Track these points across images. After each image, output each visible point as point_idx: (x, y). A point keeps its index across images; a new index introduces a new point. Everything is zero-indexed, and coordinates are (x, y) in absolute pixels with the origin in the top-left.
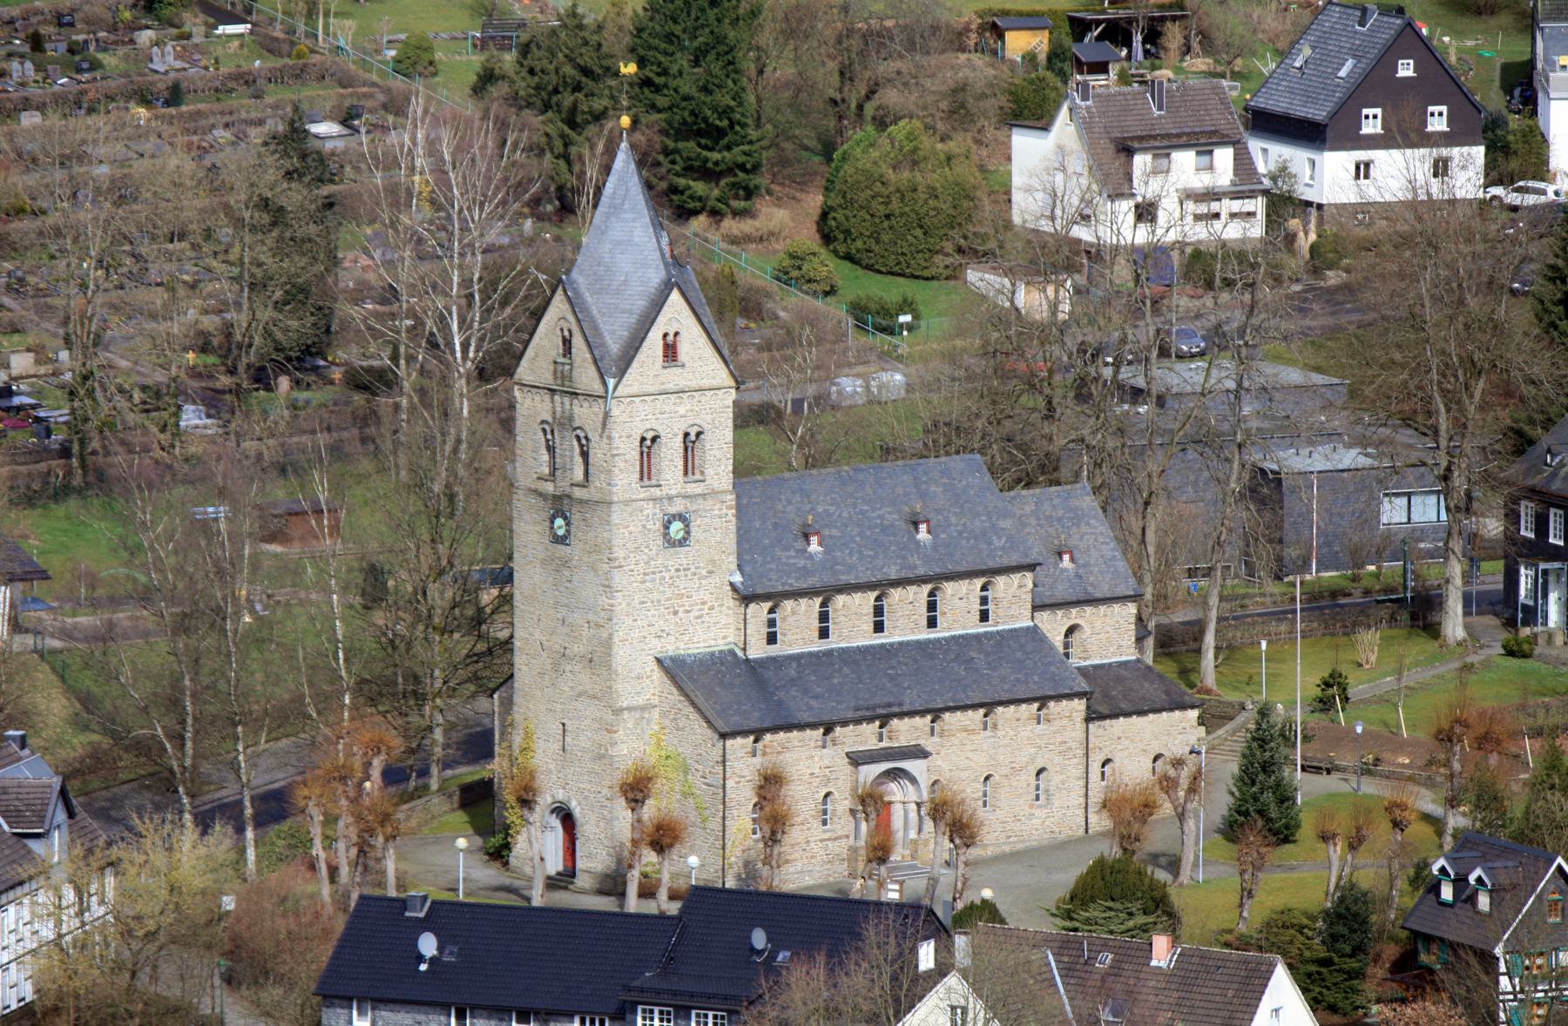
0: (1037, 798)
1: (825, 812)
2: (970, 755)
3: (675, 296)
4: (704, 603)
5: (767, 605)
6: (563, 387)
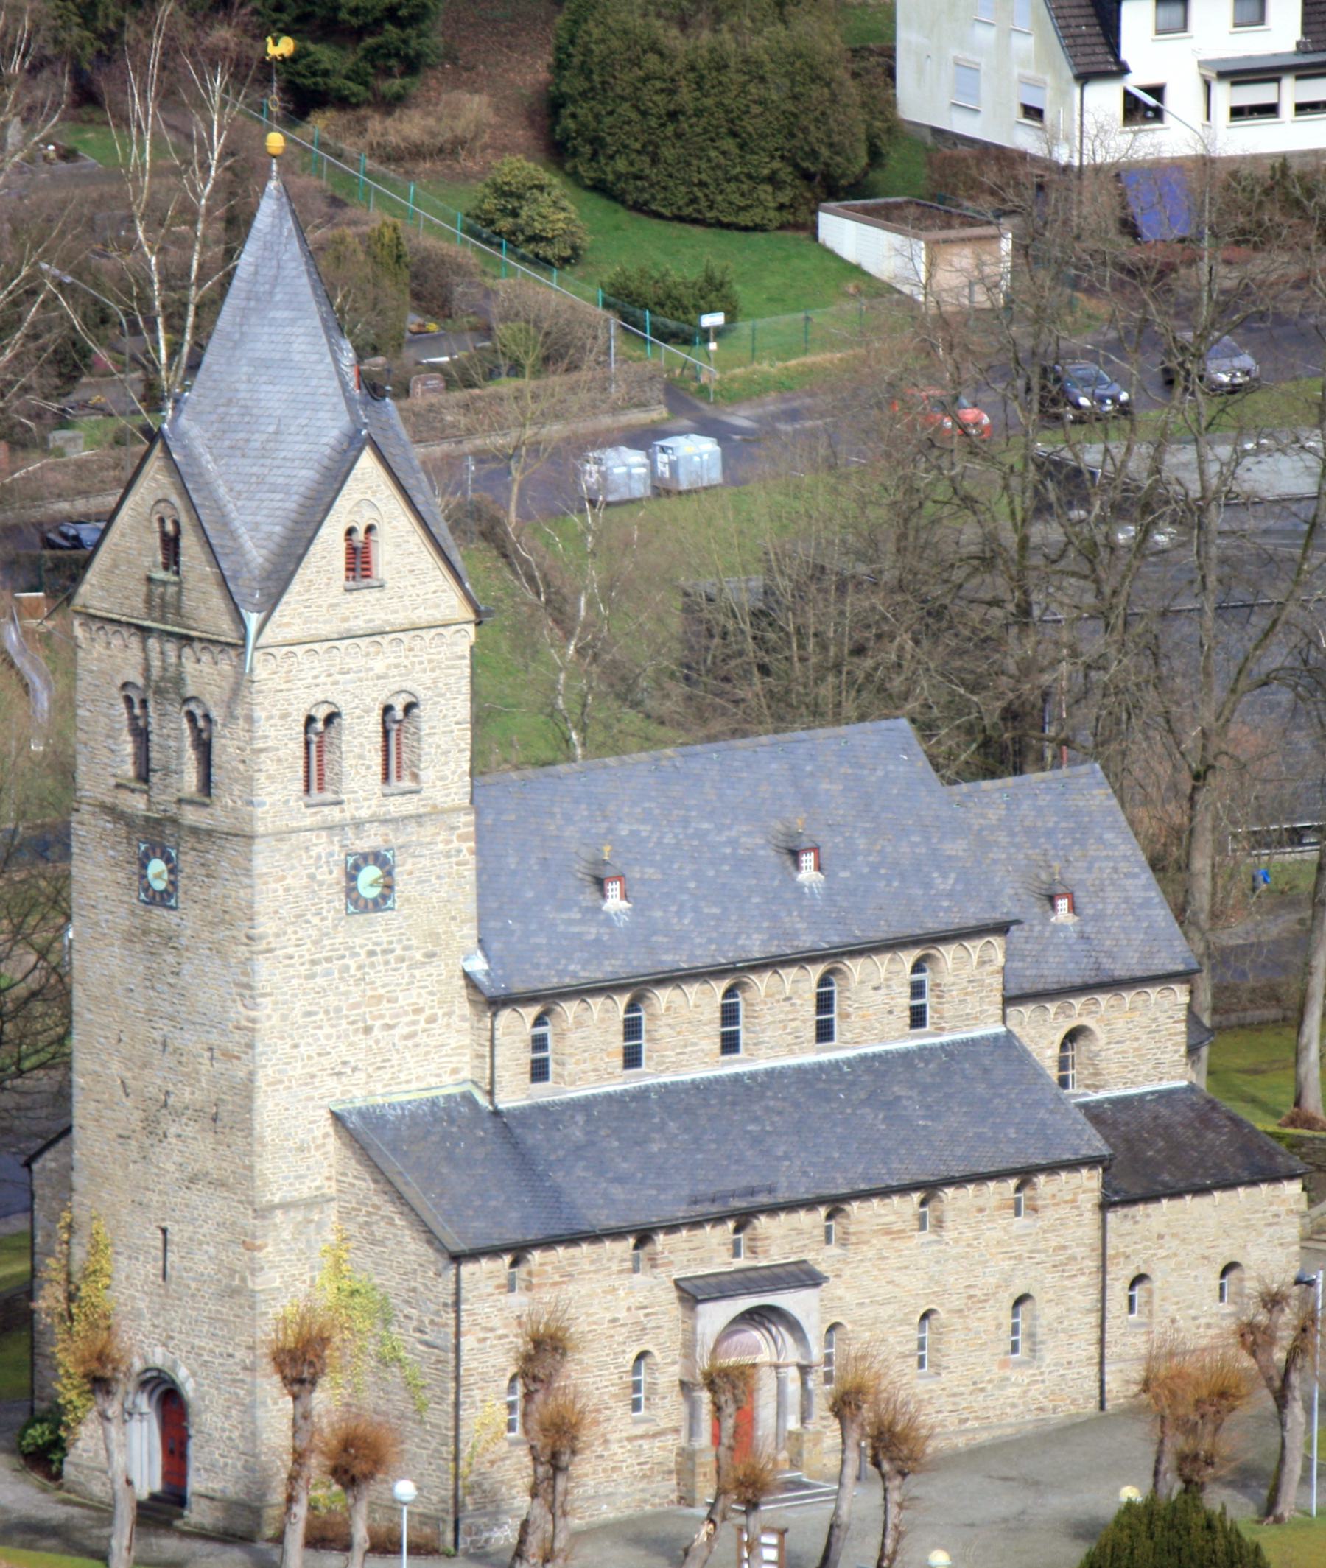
0: (1015, 1348)
1: (636, 1387)
2: (896, 1276)
3: (367, 460)
4: (418, 1011)
5: (533, 1011)
6: (162, 620)
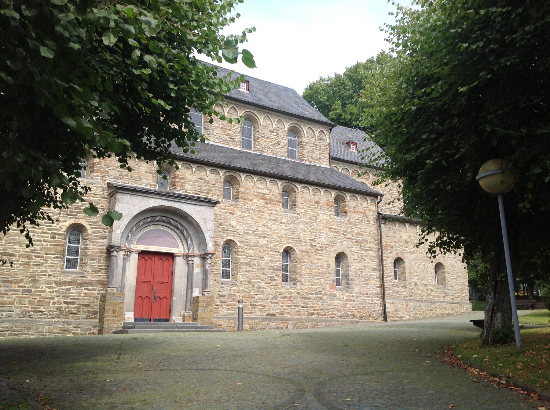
1: (73, 252)
